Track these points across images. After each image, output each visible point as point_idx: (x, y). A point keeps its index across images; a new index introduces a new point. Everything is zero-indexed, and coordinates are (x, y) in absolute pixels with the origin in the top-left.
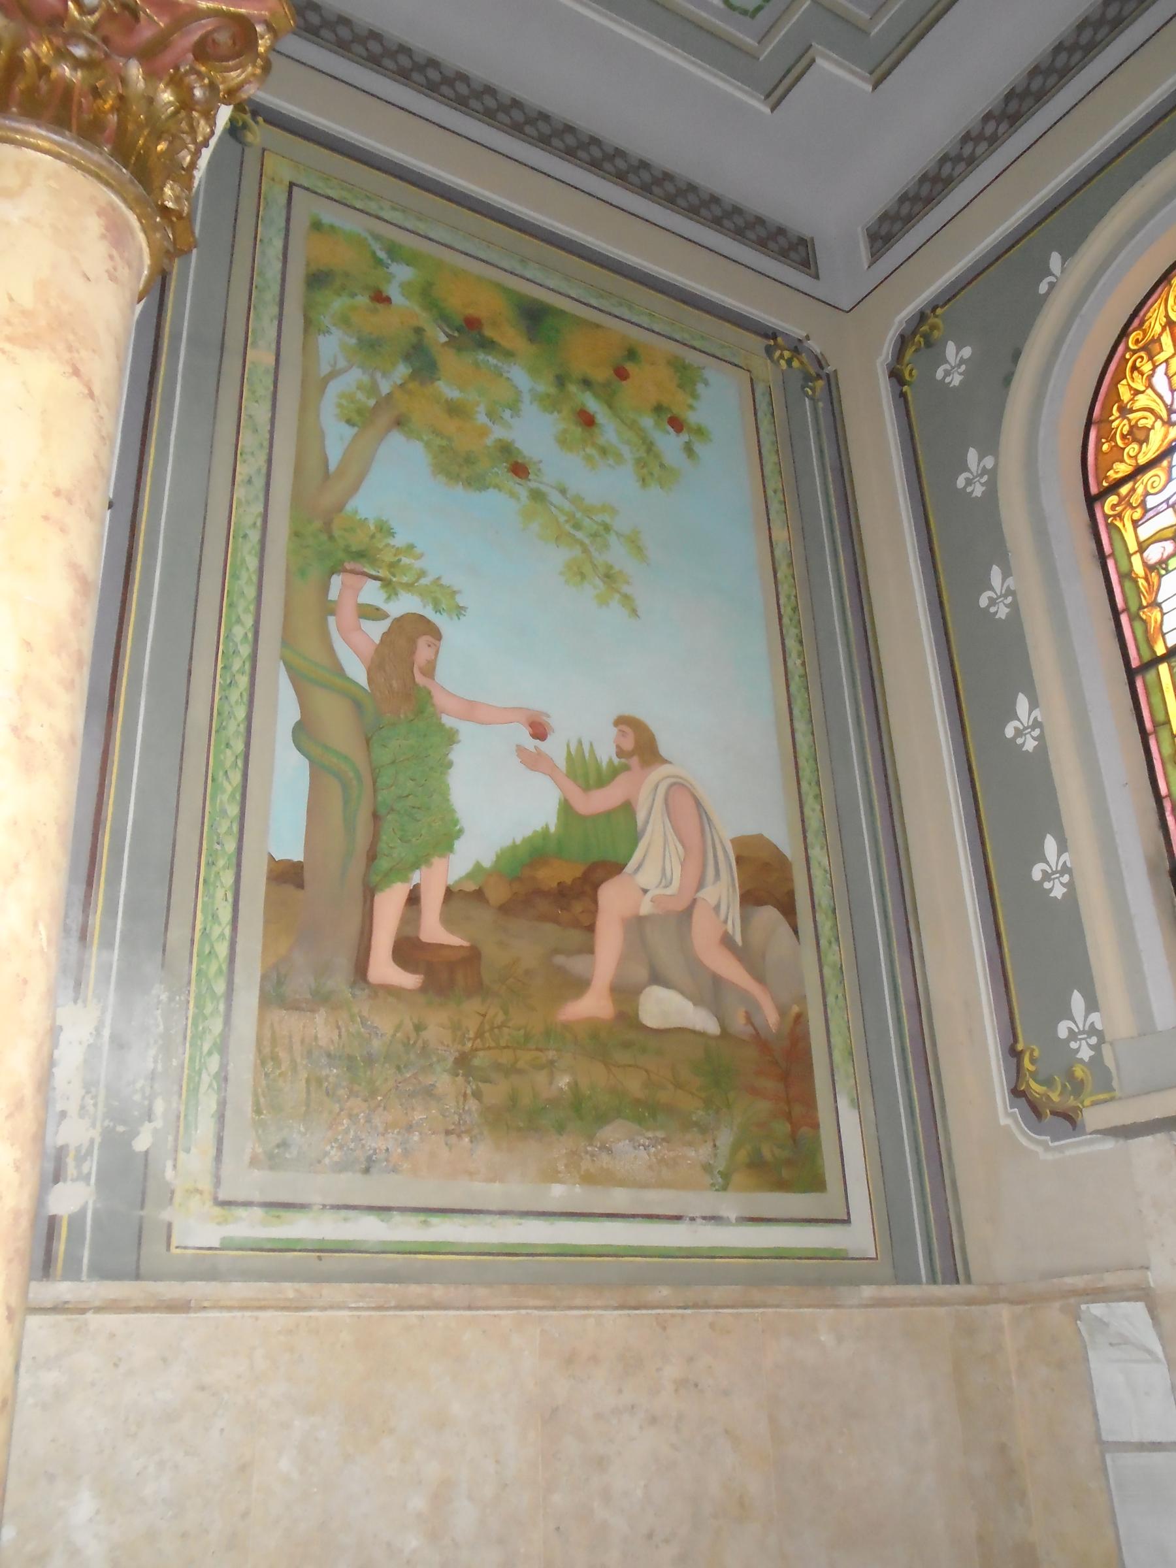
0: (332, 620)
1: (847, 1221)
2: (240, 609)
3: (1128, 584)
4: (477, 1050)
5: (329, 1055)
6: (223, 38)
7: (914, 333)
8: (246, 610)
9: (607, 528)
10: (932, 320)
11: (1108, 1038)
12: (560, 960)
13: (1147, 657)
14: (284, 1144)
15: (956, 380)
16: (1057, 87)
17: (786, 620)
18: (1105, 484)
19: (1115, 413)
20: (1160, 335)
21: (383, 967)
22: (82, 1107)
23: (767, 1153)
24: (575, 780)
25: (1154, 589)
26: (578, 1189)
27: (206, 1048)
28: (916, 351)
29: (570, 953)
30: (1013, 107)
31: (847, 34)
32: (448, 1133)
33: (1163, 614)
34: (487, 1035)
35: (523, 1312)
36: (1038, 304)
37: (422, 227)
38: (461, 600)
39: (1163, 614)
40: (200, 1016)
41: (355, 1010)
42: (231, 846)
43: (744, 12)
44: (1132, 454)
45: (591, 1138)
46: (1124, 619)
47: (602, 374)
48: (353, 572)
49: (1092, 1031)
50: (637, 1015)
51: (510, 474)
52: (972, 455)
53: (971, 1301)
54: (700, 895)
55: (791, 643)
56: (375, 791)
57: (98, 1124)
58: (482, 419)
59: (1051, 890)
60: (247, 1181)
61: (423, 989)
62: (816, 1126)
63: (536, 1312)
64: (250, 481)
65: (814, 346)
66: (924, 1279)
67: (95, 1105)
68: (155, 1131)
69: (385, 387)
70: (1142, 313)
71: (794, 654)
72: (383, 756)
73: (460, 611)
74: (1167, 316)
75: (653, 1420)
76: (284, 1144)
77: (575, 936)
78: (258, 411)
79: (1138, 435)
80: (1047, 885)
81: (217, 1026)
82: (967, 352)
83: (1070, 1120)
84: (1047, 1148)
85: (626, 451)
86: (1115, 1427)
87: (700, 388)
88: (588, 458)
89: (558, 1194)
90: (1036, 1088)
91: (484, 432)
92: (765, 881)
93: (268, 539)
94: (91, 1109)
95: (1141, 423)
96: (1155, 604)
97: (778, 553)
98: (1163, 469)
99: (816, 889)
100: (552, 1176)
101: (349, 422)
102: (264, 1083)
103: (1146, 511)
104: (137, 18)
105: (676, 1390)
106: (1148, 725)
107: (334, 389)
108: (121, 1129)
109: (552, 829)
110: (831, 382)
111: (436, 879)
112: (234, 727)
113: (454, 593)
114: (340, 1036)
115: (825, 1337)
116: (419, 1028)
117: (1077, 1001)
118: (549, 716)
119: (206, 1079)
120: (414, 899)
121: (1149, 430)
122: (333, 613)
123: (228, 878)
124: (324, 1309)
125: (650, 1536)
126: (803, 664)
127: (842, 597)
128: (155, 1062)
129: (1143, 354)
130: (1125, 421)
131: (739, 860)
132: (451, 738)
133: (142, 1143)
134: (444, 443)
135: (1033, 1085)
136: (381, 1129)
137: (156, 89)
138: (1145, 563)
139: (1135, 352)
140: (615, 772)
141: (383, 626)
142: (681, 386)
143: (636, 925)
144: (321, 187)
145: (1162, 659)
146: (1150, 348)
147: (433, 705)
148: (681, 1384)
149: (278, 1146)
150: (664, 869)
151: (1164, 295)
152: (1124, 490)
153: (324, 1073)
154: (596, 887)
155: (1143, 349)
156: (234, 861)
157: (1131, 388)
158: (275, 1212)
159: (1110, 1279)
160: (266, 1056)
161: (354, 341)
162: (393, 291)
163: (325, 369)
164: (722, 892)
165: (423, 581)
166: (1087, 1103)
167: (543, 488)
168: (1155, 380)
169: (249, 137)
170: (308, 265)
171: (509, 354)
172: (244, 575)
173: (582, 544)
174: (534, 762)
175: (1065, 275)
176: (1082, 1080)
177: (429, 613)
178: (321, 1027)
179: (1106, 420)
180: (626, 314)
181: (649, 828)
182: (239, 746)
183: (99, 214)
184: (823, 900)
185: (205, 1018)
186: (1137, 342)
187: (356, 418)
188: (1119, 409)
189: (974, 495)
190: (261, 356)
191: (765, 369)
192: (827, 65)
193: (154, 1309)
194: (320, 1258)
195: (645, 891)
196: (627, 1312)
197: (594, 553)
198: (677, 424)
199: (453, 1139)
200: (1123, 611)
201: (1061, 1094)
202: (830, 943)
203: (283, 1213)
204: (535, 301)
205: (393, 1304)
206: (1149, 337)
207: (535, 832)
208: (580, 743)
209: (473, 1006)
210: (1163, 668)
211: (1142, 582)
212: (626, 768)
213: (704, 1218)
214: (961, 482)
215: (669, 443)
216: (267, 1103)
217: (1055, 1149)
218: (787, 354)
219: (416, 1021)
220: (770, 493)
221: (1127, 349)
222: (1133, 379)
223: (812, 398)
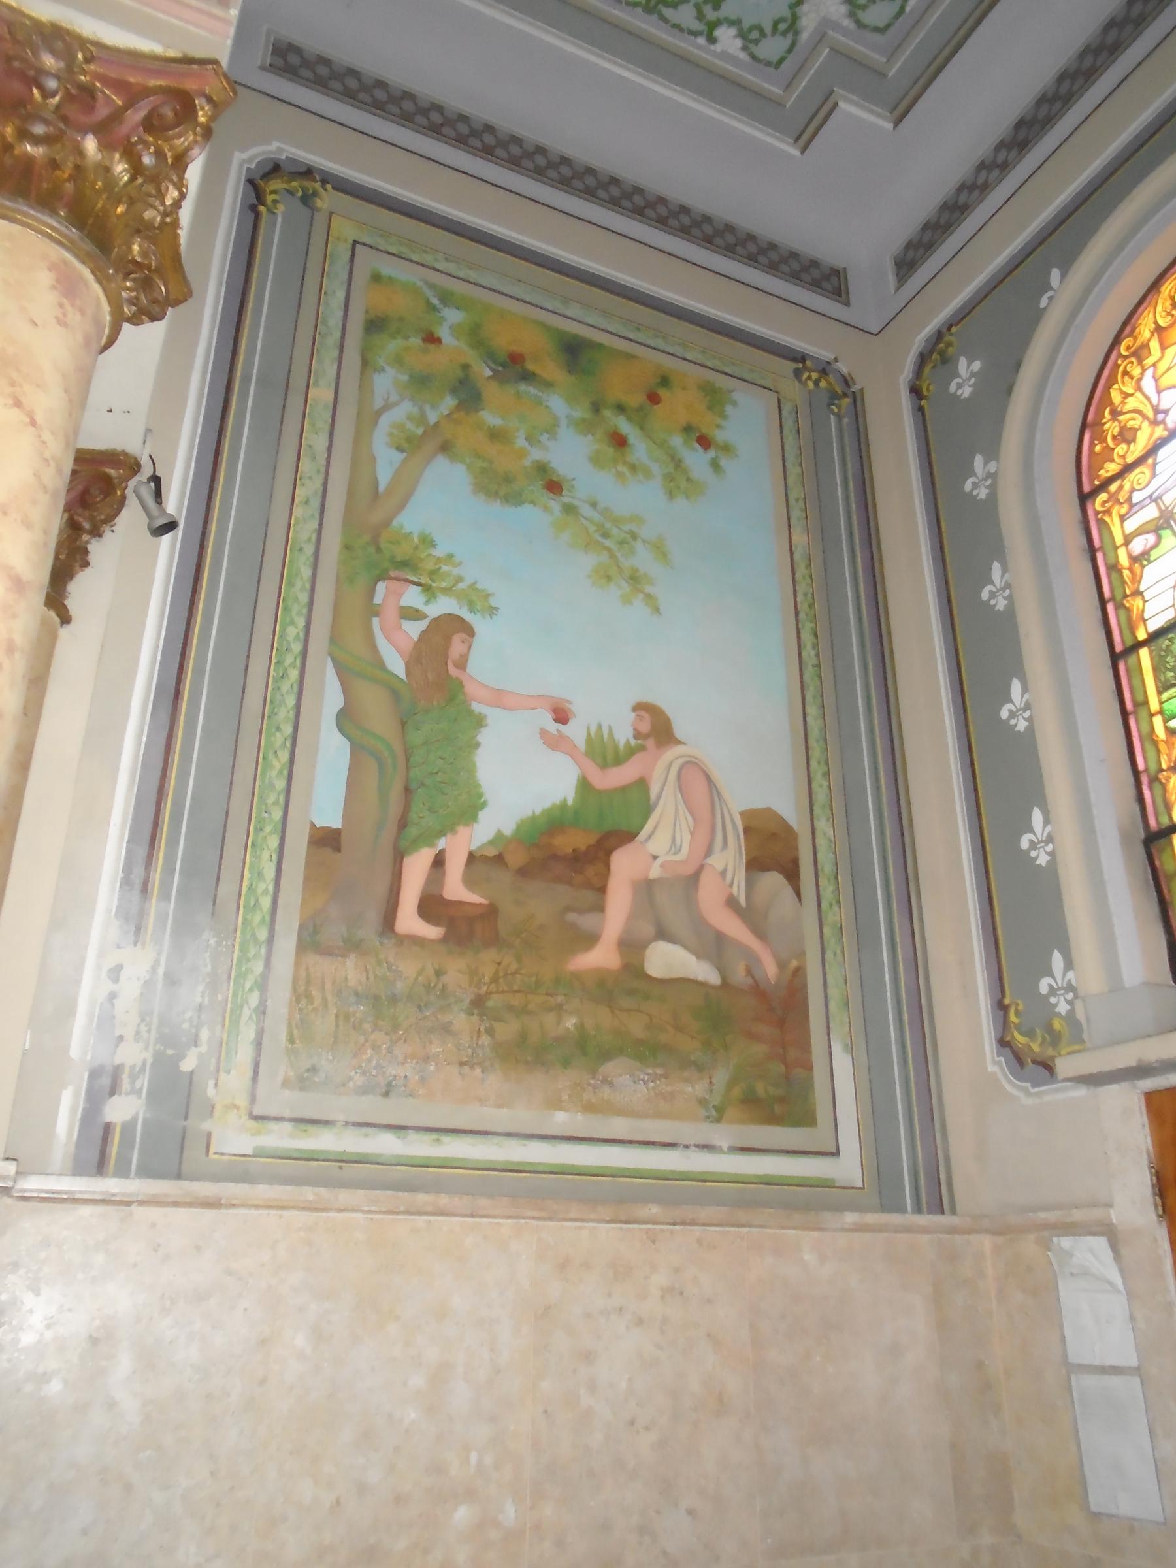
0: (375, 621)
1: (836, 1154)
2: (294, 613)
3: (1114, 575)
4: (491, 993)
5: (357, 994)
6: (168, 112)
7: (931, 352)
8: (299, 613)
9: (634, 537)
10: (947, 338)
11: (1081, 993)
12: (571, 917)
13: (1129, 643)
14: (313, 1070)
15: (966, 392)
16: (1059, 114)
17: (802, 616)
18: (1097, 483)
20: (1149, 340)
21: (409, 920)
22: (138, 1033)
23: (760, 1089)
24: (593, 760)
25: (1136, 579)
26: (580, 1116)
27: (248, 985)
28: (934, 367)
29: (580, 911)
30: (1022, 134)
31: (865, 78)
32: (462, 1064)
34: (501, 980)
35: (523, 1221)
36: (1036, 317)
37: (473, 275)
38: (493, 602)
40: (244, 958)
41: (382, 956)
42: (277, 814)
43: (768, 64)
44: (1121, 453)
45: (593, 1073)
46: (1110, 607)
47: (635, 399)
48: (397, 579)
49: (1070, 988)
50: (643, 967)
51: (545, 491)
52: (979, 460)
53: (953, 1230)
54: (709, 861)
55: (807, 636)
56: (408, 768)
57: (151, 1048)
58: (521, 442)
59: (1036, 858)
60: (278, 1098)
61: (445, 939)
62: (809, 1068)
63: (534, 1222)
64: (307, 503)
66: (909, 1209)
67: (149, 1031)
68: (201, 1056)
69: (433, 417)
71: (809, 646)
72: (416, 738)
73: (492, 611)
75: (640, 1322)
76: (313, 1070)
77: (590, 896)
78: (318, 442)
79: (1127, 436)
81: (259, 967)
82: (977, 366)
84: (1028, 1094)
85: (655, 468)
86: (1078, 1353)
87: (729, 409)
88: (620, 475)
89: (561, 1120)
90: (1020, 1039)
91: (522, 454)
92: (771, 849)
93: (322, 551)
94: (145, 1035)
95: (1131, 424)
96: (1138, 593)
97: (797, 556)
99: (820, 856)
100: (555, 1104)
101: (399, 449)
102: (297, 1016)
103: (1132, 506)
104: (93, 97)
105: (663, 1297)
106: (1129, 706)
107: (385, 421)
108: (170, 1052)
109: (570, 802)
110: (857, 399)
111: (459, 845)
112: (285, 713)
113: (488, 595)
114: (368, 978)
115: (809, 1257)
116: (439, 973)
117: (1057, 959)
118: (570, 703)
119: (246, 1012)
120: (439, 862)
122: (377, 614)
123: (274, 842)
124: (340, 1210)
125: (632, 1423)
126: (818, 655)
127: (858, 598)
128: (202, 996)
129: (1133, 359)
130: (1116, 423)
131: (747, 830)
132: (480, 722)
133: (187, 1065)
134: (485, 465)
135: (1016, 1034)
136: (401, 1058)
137: (112, 158)
139: (1126, 357)
140: (631, 752)
141: (422, 625)
142: (710, 408)
143: (646, 889)
144: (382, 244)
146: (1140, 353)
147: (464, 694)
148: (668, 1292)
149: (308, 1070)
150: (674, 839)
151: (1153, 303)
152: (1113, 487)
153: (351, 1009)
154: (609, 853)
156: (279, 827)
157: (1122, 392)
158: (303, 1126)
159: (1078, 1215)
160: (301, 993)
161: (405, 378)
162: (444, 333)
163: (378, 403)
164: (729, 859)
165: (461, 586)
166: (1063, 1052)
167: (576, 502)
169: (319, 203)
170: (367, 312)
171: (548, 385)
172: (299, 584)
173: (609, 550)
174: (554, 743)
175: (1063, 289)
177: (464, 613)
178: (351, 970)
179: (1099, 423)
180: (660, 343)
181: (661, 802)
182: (288, 730)
183: (50, 270)
184: (826, 866)
185: (248, 960)
186: (1128, 348)
187: (406, 445)
190: (322, 394)
191: (792, 390)
192: (849, 108)
193: (190, 1205)
194: (341, 1168)
195: (655, 858)
196: (619, 1225)
197: (620, 558)
198: (705, 442)
199: (466, 1069)
200: (1110, 600)
201: (1042, 1044)
202: (831, 905)
203: (311, 1128)
204: (575, 337)
205: (402, 1209)
206: (1138, 343)
207: (554, 805)
208: (600, 726)
209: (489, 957)
210: (1144, 653)
211: (1126, 573)
212: (642, 748)
213: (697, 1146)
214: (968, 486)
215: (696, 460)
216: (300, 1032)
219: (437, 967)
220: (792, 502)
221: (1120, 355)
222: (1123, 383)
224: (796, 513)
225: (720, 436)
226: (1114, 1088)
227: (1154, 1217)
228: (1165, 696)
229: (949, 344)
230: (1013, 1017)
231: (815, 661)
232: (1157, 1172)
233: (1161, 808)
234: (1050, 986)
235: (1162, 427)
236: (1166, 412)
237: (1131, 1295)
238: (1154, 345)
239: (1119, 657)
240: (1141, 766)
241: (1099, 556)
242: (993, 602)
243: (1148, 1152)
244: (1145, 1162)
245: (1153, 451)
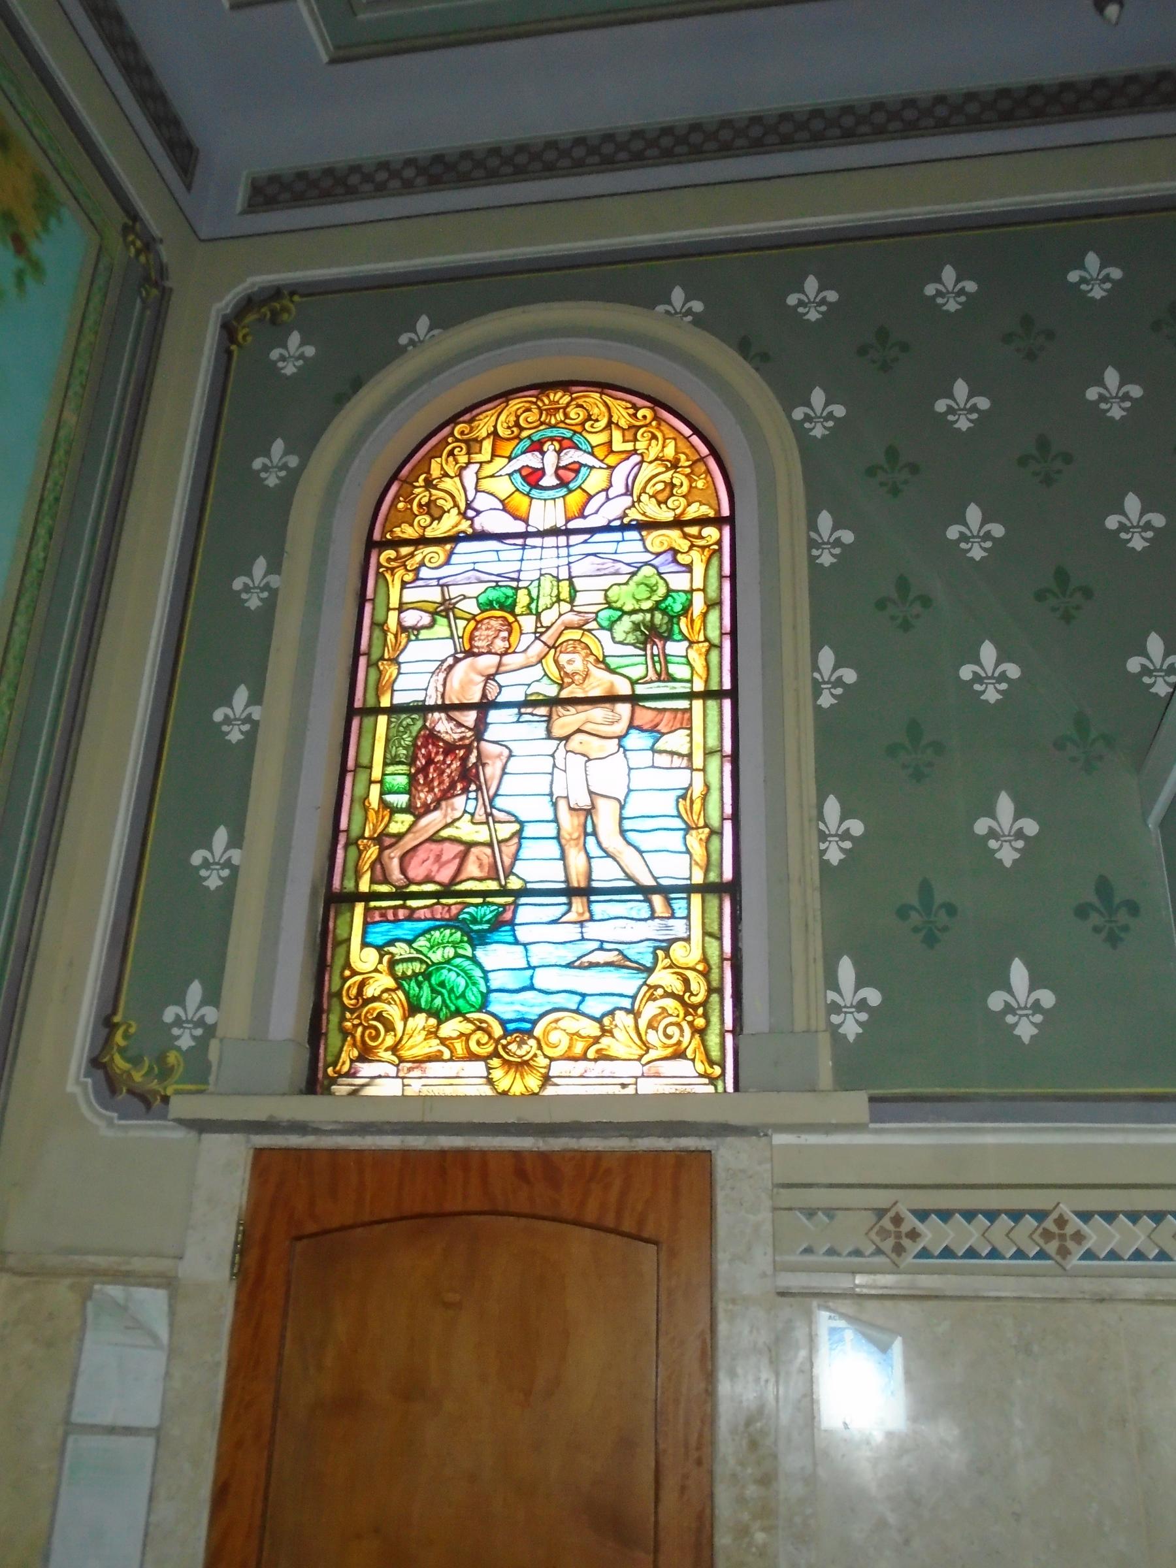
3: (377, 633)
7: (264, 302)
10: (286, 302)
13: (371, 703)
15: (289, 369)
17: (45, 507)
18: (388, 536)
19: (421, 481)
20: (484, 439)
33: (399, 673)
39: (399, 673)
44: (423, 524)
46: (363, 661)
52: (278, 446)
55: (42, 532)
65: (164, 252)
70: (475, 412)
71: (41, 544)
74: (495, 427)
79: (434, 512)
80: (203, 873)
83: (148, 1103)
90: (120, 1063)
95: (440, 502)
96: (395, 661)
98: (445, 551)
103: (417, 579)
106: (351, 764)
110: (166, 293)
121: (445, 512)
126: (45, 559)
129: (463, 445)
130: (427, 493)
138: (399, 623)
139: (457, 440)
145: (384, 711)
146: (472, 445)
151: (499, 409)
152: (405, 551)
155: (466, 442)
157: (442, 468)
159: (137, 1264)
168: (466, 473)
176: (173, 1066)
179: (410, 483)
186: (462, 433)
188: (425, 480)
189: (266, 482)
200: (364, 654)
210: (382, 720)
211: (390, 637)
217: (120, 1126)
218: (139, 244)
220: (76, 372)
221: (452, 434)
223: (143, 301)
224: (76, 387)
225: (36, 248)
226: (225, 1137)
227: (226, 1273)
228: (390, 769)
229: (285, 309)
230: (119, 1038)
231: (40, 566)
232: (244, 1232)
233: (350, 873)
234: (178, 1016)
235: (469, 522)
236: (478, 513)
237: (173, 1352)
238: (487, 445)
239: (356, 712)
240: (343, 825)
241: (368, 608)
242: (244, 596)
243: (240, 1208)
244: (234, 1219)
245: (455, 539)
